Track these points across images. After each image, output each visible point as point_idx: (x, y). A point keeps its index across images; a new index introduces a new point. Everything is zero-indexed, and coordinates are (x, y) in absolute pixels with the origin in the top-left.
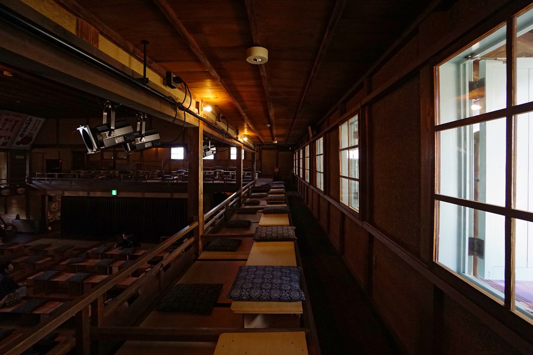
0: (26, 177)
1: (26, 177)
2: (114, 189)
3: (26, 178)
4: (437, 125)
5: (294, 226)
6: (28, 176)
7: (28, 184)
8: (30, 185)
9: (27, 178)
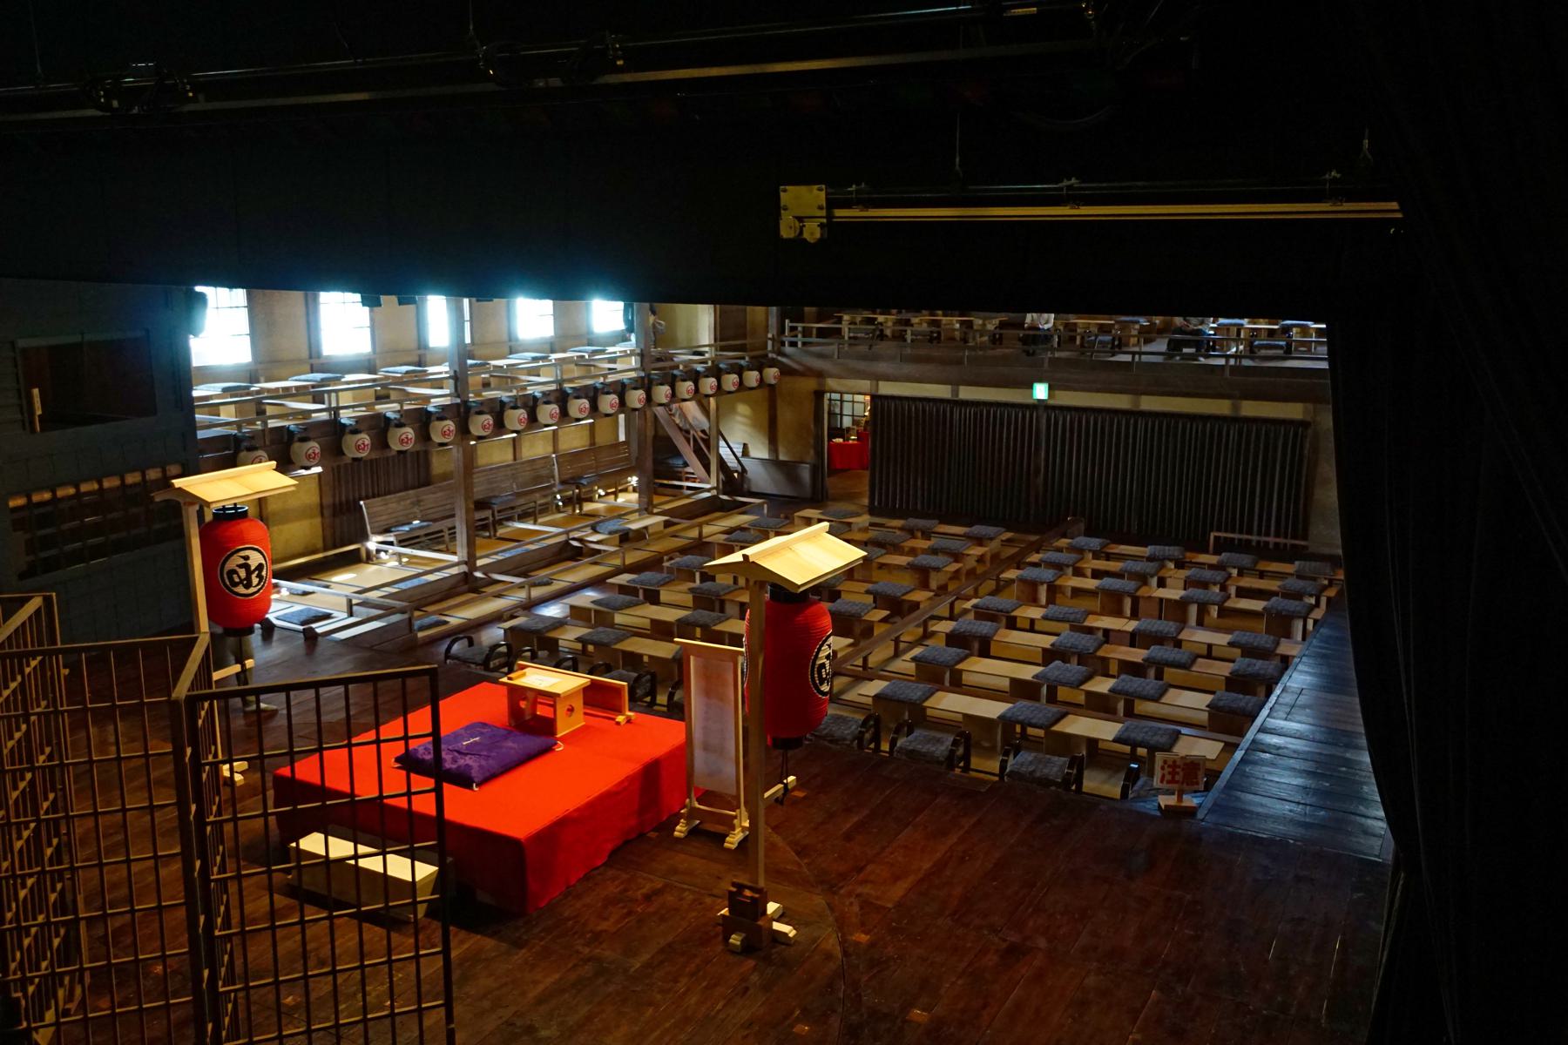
0: (770, 336)
1: (770, 336)
2: (1040, 381)
3: (770, 339)
4: (197, 416)
5: (760, 927)
6: (775, 333)
7: (774, 356)
8: (779, 358)
9: (773, 339)
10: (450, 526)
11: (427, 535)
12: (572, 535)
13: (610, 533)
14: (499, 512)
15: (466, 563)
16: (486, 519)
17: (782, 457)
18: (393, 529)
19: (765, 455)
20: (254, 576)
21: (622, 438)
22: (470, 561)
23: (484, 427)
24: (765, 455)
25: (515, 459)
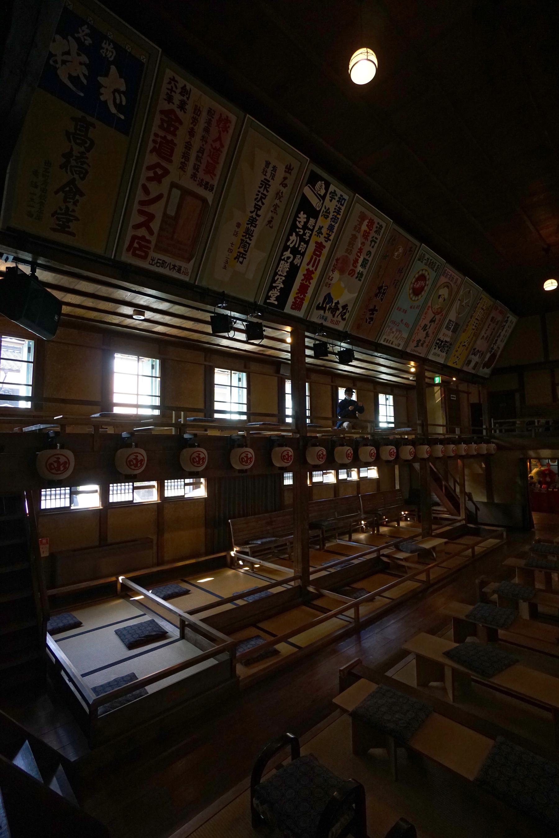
0: (484, 427)
9: (486, 429)
10: (454, 355)
11: (276, 547)
12: (382, 552)
13: (412, 552)
14: (326, 531)
15: (300, 578)
16: (318, 536)
17: (496, 501)
18: (250, 542)
19: (485, 500)
20: (61, 467)
21: (397, 487)
22: (304, 575)
23: (319, 457)
24: (485, 500)
25: (335, 496)
